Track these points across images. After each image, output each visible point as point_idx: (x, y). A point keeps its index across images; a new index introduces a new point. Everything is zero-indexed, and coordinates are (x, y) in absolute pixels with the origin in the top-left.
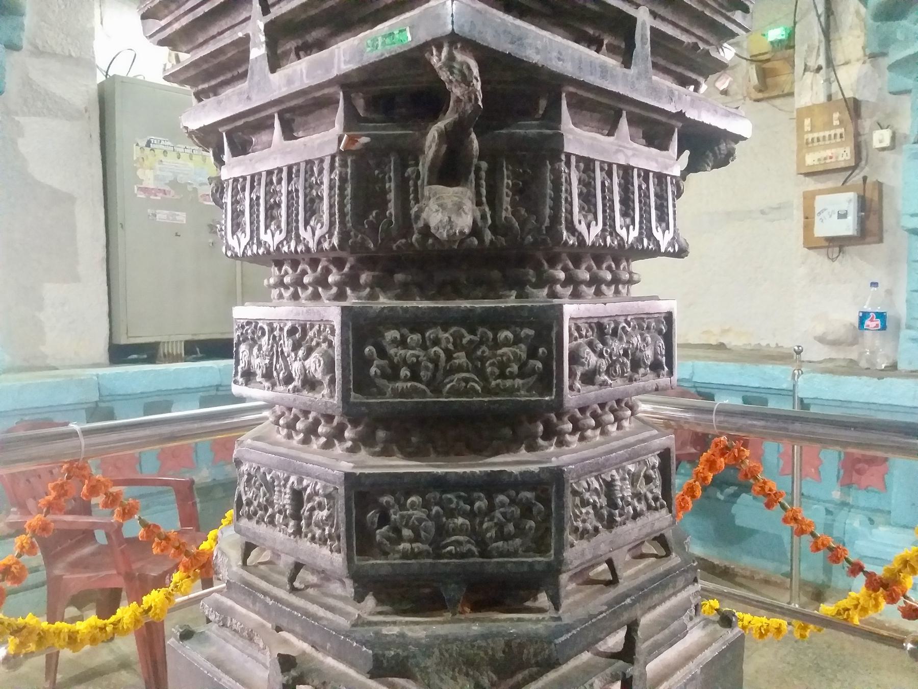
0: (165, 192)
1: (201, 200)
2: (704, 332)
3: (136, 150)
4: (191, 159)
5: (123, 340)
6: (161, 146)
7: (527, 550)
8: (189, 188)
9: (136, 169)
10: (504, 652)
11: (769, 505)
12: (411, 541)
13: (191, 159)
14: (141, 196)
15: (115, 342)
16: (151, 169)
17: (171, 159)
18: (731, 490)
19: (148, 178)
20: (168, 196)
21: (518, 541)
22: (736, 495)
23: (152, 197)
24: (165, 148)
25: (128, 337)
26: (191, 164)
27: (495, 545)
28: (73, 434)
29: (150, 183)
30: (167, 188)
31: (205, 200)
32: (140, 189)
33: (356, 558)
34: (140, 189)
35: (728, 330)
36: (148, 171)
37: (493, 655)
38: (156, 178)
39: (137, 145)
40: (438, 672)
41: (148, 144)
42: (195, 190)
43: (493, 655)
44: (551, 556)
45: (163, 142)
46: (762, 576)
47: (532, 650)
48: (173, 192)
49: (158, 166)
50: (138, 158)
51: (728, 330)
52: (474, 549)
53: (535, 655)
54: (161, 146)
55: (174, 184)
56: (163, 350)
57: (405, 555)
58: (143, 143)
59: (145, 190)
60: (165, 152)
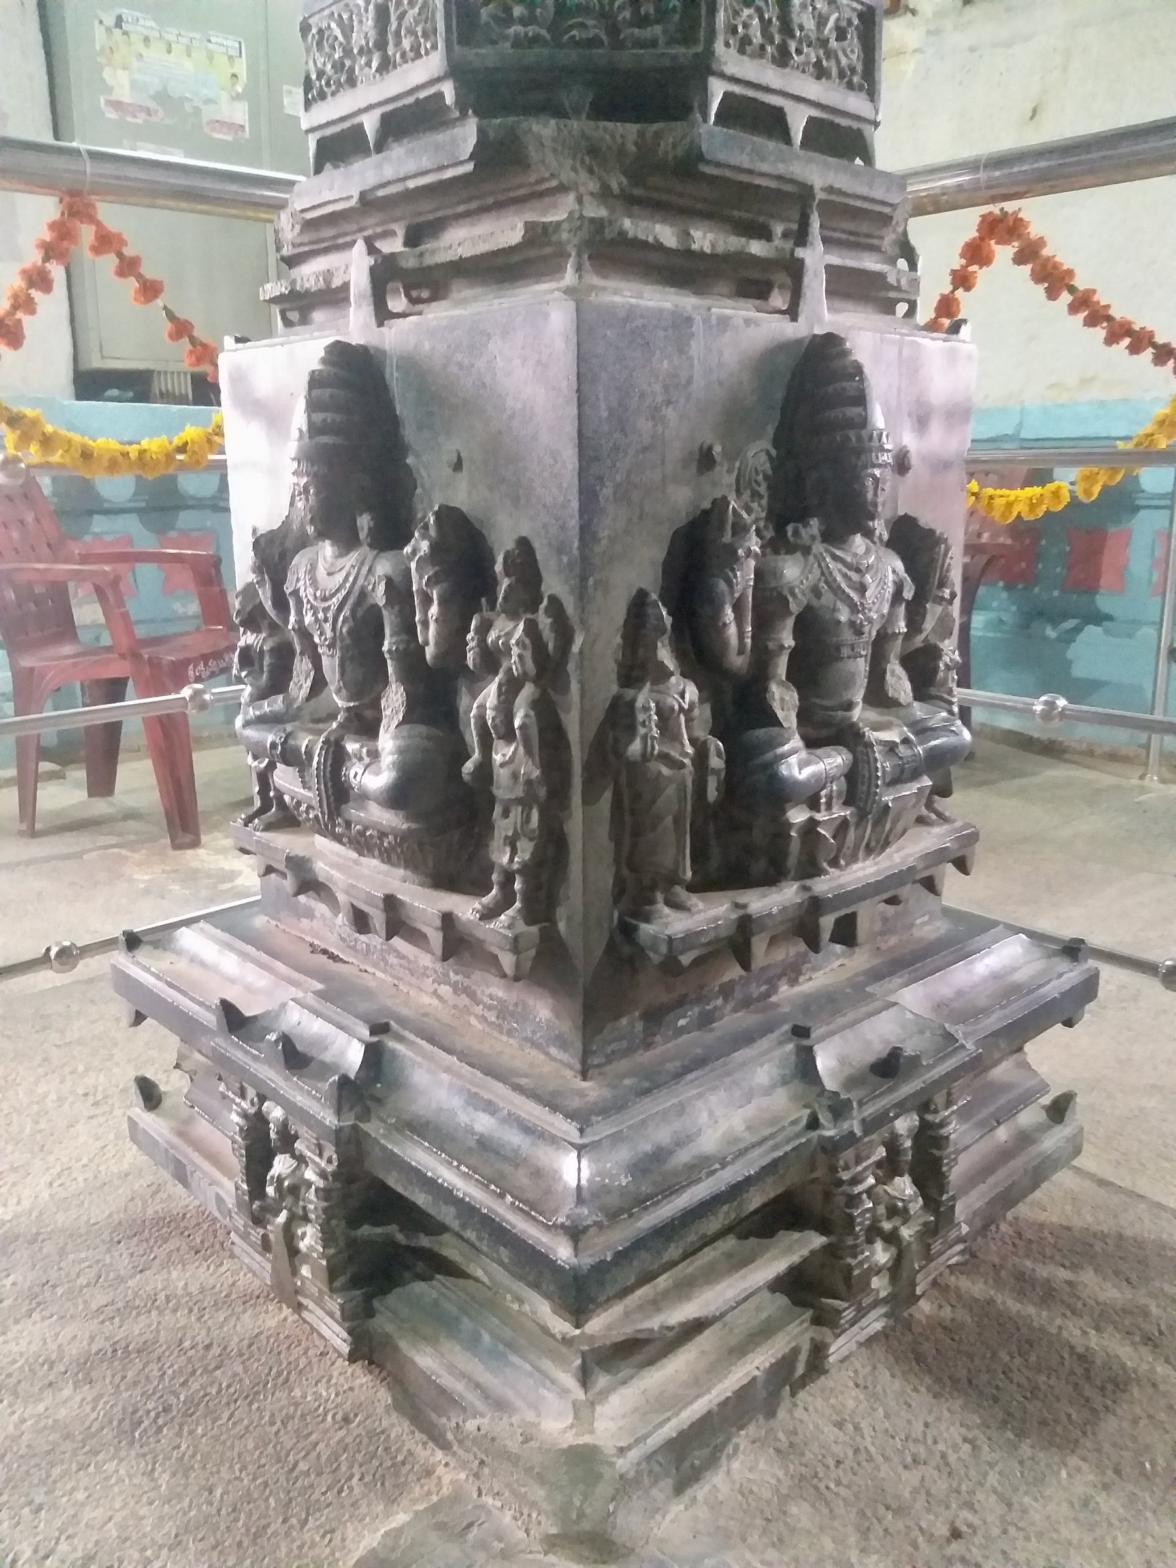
0: (148, 112)
1: (206, 130)
2: (1052, 386)
3: (99, 31)
4: (189, 55)
5: (95, 362)
6: (139, 28)
7: (671, 42)
8: (188, 108)
9: (101, 68)
10: (636, 144)
11: (1052, 294)
12: (523, 22)
13: (189, 55)
14: (112, 115)
15: (83, 367)
16: (125, 68)
17: (154, 53)
18: (1071, 624)
19: (121, 85)
20: (154, 119)
21: (657, 29)
22: (1077, 630)
23: (130, 119)
24: (146, 33)
25: (103, 357)
26: (188, 65)
27: (629, 31)
28: (77, 152)
29: (124, 94)
30: (152, 104)
31: (213, 130)
32: (109, 103)
33: (456, 47)
34: (109, 103)
35: (1092, 380)
36: (120, 72)
37: (623, 144)
38: (134, 85)
39: (101, 22)
40: (555, 150)
41: (119, 22)
42: (197, 111)
43: (623, 144)
44: (700, 49)
45: (141, 22)
46: (1106, 749)
47: (671, 140)
48: (161, 113)
49: (135, 64)
50: (103, 48)
51: (1092, 380)
52: (604, 37)
53: (674, 146)
54: (139, 28)
55: (163, 97)
56: (158, 386)
57: (517, 43)
58: (110, 21)
59: (117, 105)
60: (147, 40)
